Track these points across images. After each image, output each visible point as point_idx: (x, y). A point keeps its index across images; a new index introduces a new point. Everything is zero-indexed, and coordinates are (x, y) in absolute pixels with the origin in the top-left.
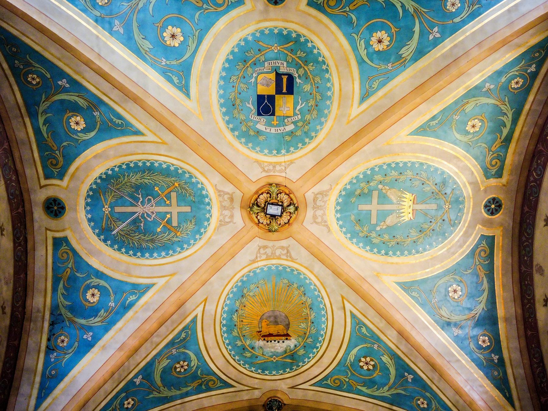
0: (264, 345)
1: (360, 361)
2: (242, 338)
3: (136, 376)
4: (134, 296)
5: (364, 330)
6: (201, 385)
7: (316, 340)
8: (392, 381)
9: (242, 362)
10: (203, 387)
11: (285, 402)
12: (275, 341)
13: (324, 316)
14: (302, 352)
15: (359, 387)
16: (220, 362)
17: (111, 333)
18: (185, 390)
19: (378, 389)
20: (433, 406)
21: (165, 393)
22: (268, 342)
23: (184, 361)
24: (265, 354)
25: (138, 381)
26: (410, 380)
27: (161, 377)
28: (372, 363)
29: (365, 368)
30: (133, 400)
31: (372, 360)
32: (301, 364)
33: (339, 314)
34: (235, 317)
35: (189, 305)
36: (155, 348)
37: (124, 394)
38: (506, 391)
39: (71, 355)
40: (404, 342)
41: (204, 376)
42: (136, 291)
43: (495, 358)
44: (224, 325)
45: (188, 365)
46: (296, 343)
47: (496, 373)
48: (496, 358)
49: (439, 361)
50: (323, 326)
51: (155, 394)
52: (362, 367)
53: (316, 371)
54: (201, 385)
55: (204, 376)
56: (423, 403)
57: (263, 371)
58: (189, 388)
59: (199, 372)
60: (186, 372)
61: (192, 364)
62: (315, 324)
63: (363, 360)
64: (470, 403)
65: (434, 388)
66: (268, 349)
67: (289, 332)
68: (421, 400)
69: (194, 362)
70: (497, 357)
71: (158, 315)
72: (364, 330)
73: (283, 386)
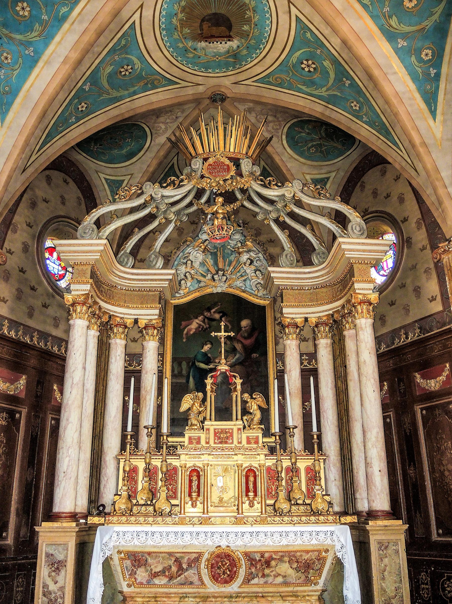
0: (207, 46)
1: (302, 63)
2: (183, 40)
3: (84, 83)
4: (65, 7)
5: (308, 35)
6: (147, 84)
7: (259, 42)
8: (330, 84)
9: (185, 62)
10: (149, 86)
11: (228, 96)
12: (217, 42)
13: (268, 19)
14: (245, 52)
15: (299, 86)
16: (164, 63)
17: (51, 48)
18: (132, 90)
19: (316, 89)
20: (364, 110)
21: (114, 94)
22: (210, 43)
23: (128, 66)
24: (207, 54)
25: (87, 88)
26: (347, 85)
27: (108, 81)
28: (314, 66)
29: (307, 69)
30: (85, 104)
31: (313, 63)
32: (244, 63)
33: (284, 18)
34: (174, 21)
35: (125, 14)
36: (97, 57)
37: (77, 100)
38: (433, 105)
39: (18, 71)
40: (346, 50)
41: (149, 76)
42: (67, 2)
43: (432, 72)
44: (163, 29)
45: (132, 69)
46: (239, 44)
47: (428, 87)
48: (433, 72)
49: (376, 73)
50: (267, 29)
51: (105, 96)
52: (303, 69)
53: (258, 69)
54: (147, 84)
55: (149, 76)
56: (355, 106)
57: (206, 69)
58: (136, 88)
59: (144, 73)
60: (131, 74)
61: (136, 67)
62: (259, 26)
63: (305, 62)
64: (396, 113)
65: (368, 95)
66: (211, 50)
67: (231, 34)
68: (355, 103)
69: (138, 65)
70: (435, 71)
71: (95, 26)
72: (308, 35)
73: (227, 82)
